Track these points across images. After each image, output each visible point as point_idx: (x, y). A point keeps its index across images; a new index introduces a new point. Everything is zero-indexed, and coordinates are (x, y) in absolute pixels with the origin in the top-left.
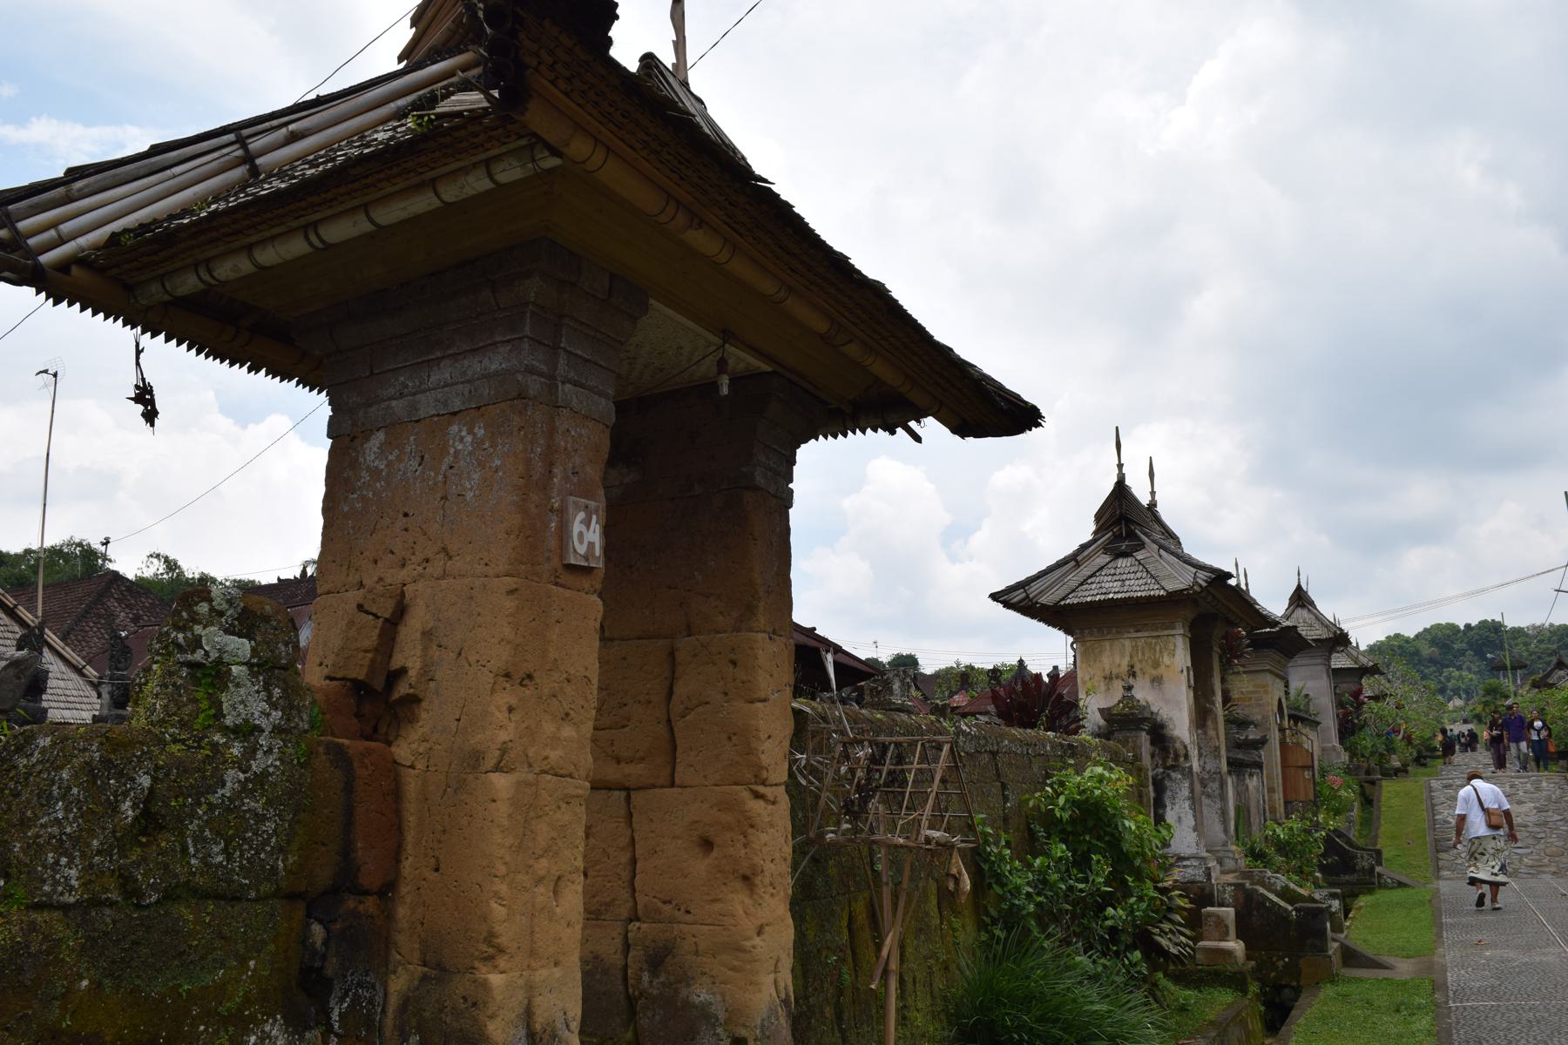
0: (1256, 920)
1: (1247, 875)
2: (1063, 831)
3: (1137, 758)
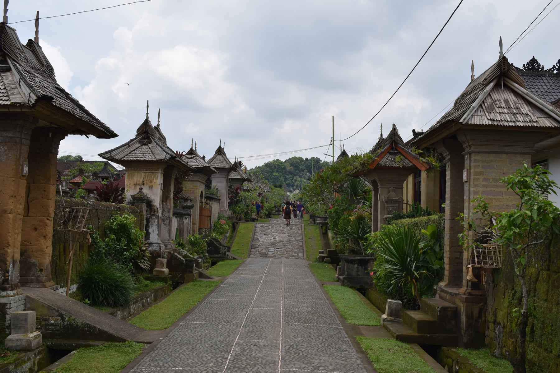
0: (172, 262)
1: (175, 251)
2: (114, 232)
3: (141, 211)
